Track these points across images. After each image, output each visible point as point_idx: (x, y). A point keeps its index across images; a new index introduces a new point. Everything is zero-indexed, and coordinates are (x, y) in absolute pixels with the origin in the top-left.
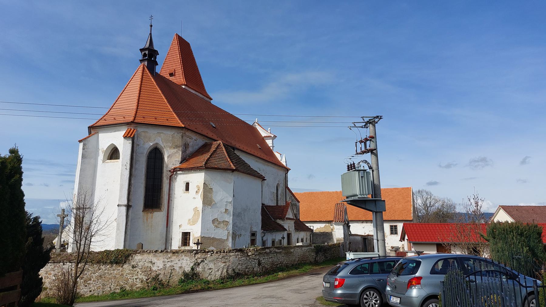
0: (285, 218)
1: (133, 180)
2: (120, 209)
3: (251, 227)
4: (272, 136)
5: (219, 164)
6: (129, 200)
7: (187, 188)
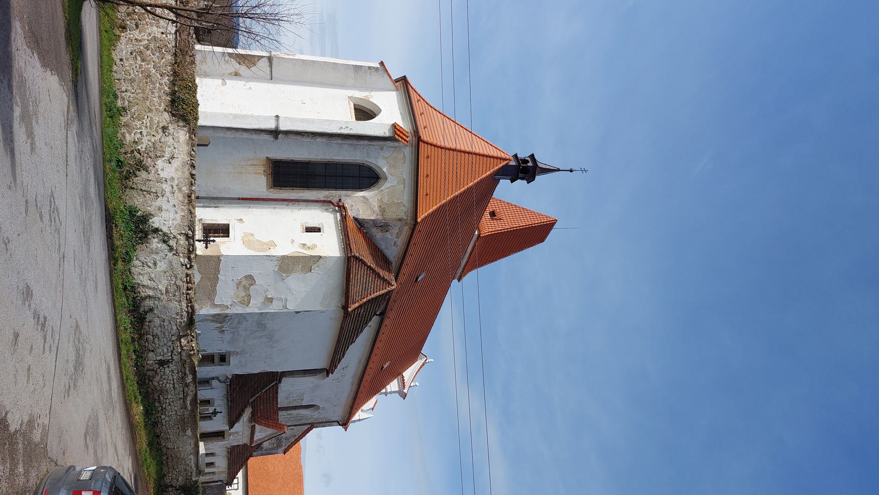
0: (255, 424)
1: (322, 141)
2: (271, 119)
3: (236, 353)
4: (405, 391)
5: (356, 283)
6: (287, 133)
7: (309, 230)
